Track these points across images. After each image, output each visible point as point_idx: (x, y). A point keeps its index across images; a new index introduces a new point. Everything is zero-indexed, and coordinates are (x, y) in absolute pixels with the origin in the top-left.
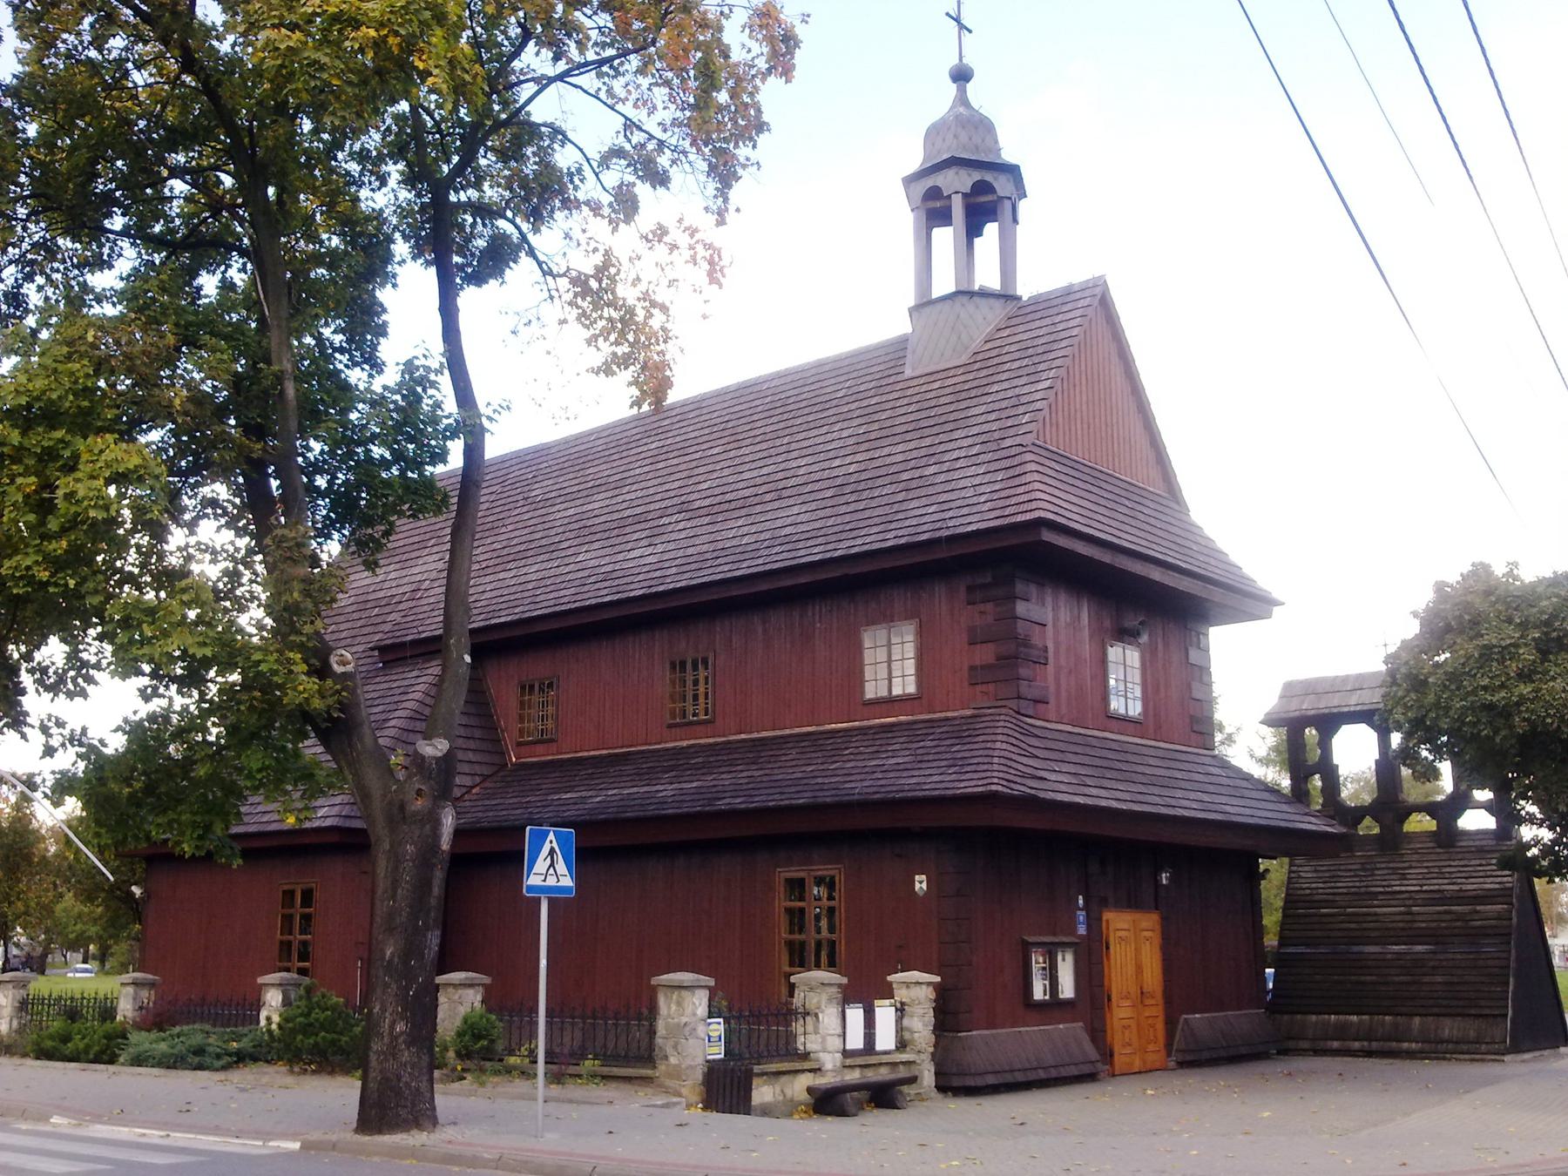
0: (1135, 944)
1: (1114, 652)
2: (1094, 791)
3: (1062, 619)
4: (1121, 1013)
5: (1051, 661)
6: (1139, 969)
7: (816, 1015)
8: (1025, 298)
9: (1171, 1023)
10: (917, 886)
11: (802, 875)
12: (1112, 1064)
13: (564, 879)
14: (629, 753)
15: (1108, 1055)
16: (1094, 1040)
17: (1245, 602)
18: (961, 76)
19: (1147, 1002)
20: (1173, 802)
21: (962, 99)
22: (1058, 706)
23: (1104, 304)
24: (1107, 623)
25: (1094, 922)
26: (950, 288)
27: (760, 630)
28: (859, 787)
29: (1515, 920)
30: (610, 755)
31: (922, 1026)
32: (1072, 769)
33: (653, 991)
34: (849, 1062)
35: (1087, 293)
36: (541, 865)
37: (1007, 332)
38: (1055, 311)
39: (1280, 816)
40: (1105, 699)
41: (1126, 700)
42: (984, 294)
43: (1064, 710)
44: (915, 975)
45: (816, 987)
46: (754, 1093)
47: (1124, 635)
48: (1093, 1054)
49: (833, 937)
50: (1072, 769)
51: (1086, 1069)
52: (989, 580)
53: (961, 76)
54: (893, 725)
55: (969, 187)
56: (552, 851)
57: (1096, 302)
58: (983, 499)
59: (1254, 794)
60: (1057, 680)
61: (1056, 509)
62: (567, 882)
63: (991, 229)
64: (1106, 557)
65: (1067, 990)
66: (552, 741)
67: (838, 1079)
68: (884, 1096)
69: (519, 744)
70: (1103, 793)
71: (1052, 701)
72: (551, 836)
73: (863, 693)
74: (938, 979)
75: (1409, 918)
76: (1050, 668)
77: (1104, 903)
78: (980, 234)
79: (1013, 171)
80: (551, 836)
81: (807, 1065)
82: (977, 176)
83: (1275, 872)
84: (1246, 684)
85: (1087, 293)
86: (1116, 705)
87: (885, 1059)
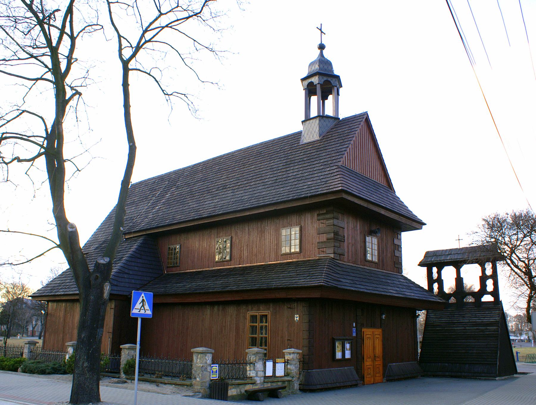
0: (373, 339)
1: (368, 239)
2: (359, 286)
3: (350, 226)
4: (368, 363)
5: (346, 241)
6: (374, 348)
7: (254, 364)
8: (341, 119)
9: (385, 366)
10: (296, 319)
11: (256, 314)
12: (364, 381)
13: (148, 311)
14: (202, 271)
15: (362, 378)
16: (357, 372)
17: (416, 224)
18: (322, 47)
19: (377, 359)
20: (387, 291)
21: (321, 54)
22: (348, 256)
23: (367, 121)
24: (366, 228)
25: (359, 332)
26: (316, 115)
27: (247, 229)
28: (274, 284)
29: (500, 332)
30: (196, 271)
31: (294, 368)
32: (351, 278)
33: (192, 353)
34: (266, 380)
35: (361, 117)
36: (138, 305)
37: (334, 130)
38: (351, 123)
39: (424, 296)
40: (365, 255)
41: (372, 254)
42: (328, 117)
43: (350, 258)
44: (292, 350)
45: (253, 353)
46: (229, 391)
47: (372, 233)
48: (356, 377)
49: (267, 336)
50: (351, 278)
51: (354, 383)
52: (325, 212)
53: (322, 47)
54: (291, 262)
55: (323, 82)
56: (143, 301)
57: (364, 120)
58: (323, 183)
59: (415, 289)
60: (348, 247)
61: (348, 187)
62: (149, 312)
63: (330, 97)
64: (365, 205)
65: (348, 355)
66: (178, 266)
67: (262, 386)
68: (273, 394)
69: (168, 267)
70: (362, 287)
71: (346, 254)
72: (143, 295)
73: (281, 251)
74: (301, 352)
75: (465, 331)
76: (346, 243)
77: (362, 326)
78: (327, 99)
79: (338, 77)
80: (143, 295)
81: (250, 381)
82: (325, 78)
83: (422, 316)
84: (413, 248)
85: (361, 117)
86: (369, 257)
87: (280, 379)
